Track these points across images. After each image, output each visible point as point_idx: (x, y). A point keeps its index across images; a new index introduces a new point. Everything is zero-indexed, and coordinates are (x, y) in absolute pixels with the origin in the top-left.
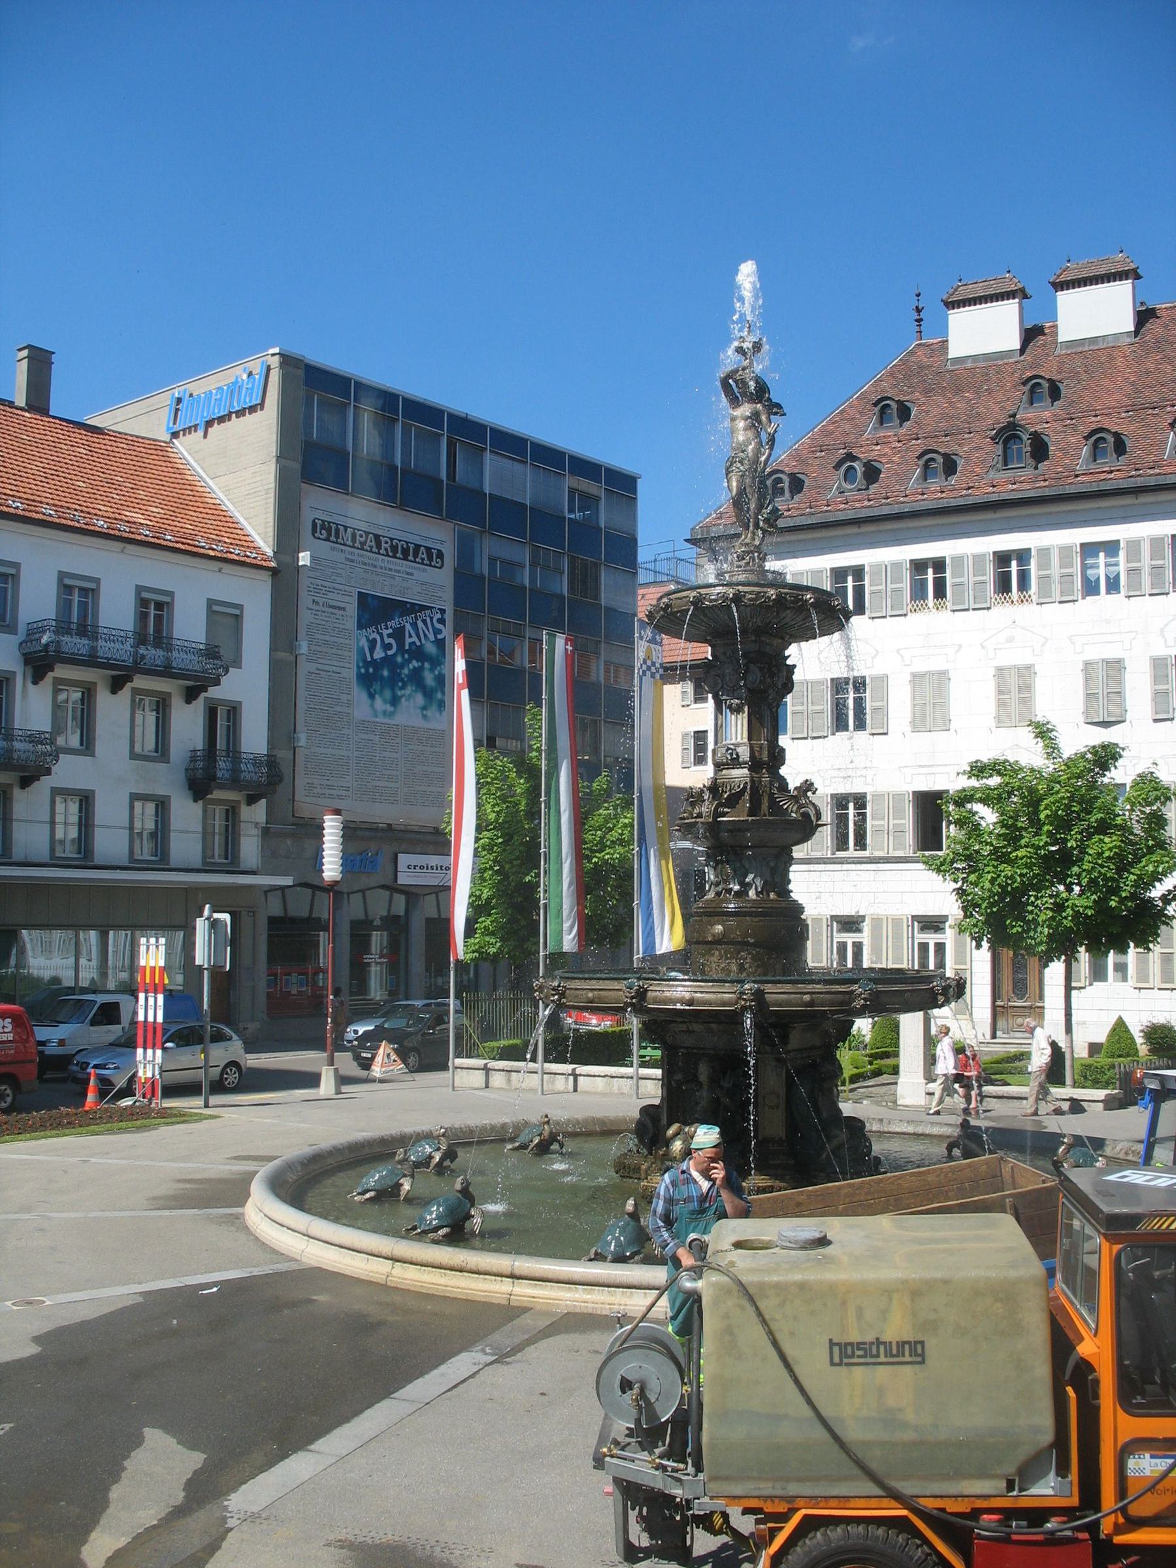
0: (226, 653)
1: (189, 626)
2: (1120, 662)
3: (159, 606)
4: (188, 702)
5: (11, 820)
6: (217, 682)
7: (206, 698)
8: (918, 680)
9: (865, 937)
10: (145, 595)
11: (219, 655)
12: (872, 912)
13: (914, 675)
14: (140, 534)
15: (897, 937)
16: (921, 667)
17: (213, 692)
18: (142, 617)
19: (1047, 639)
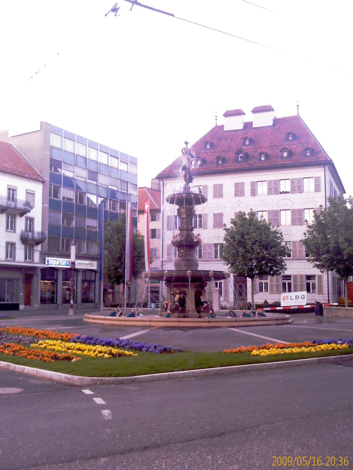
0: (31, 204)
1: (21, 197)
2: (222, 213)
3: (13, 190)
4: (21, 217)
5: (16, 248)
6: (29, 211)
7: (26, 216)
8: (215, 215)
9: (292, 281)
10: (10, 187)
11: (29, 206)
12: (293, 274)
13: (214, 214)
14: (303, 160)
15: (301, 281)
16: (216, 212)
17: (28, 215)
18: (9, 193)
19: (248, 205)
